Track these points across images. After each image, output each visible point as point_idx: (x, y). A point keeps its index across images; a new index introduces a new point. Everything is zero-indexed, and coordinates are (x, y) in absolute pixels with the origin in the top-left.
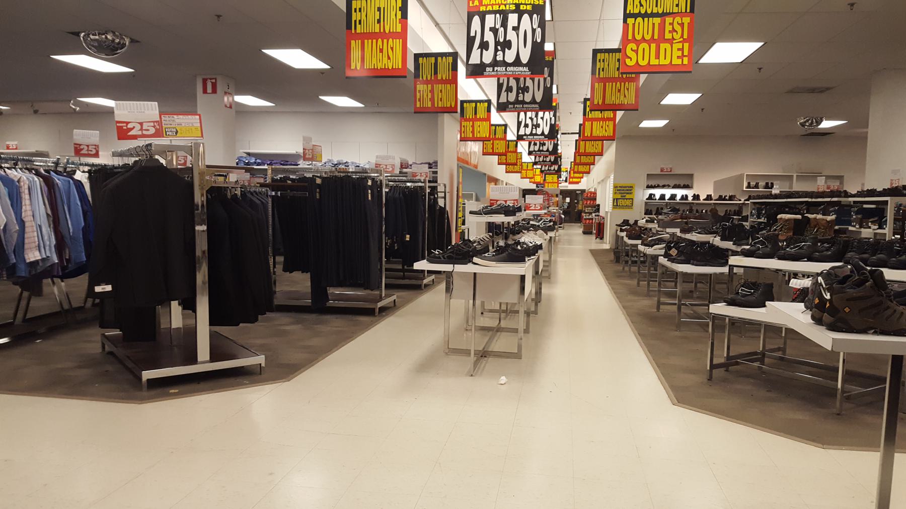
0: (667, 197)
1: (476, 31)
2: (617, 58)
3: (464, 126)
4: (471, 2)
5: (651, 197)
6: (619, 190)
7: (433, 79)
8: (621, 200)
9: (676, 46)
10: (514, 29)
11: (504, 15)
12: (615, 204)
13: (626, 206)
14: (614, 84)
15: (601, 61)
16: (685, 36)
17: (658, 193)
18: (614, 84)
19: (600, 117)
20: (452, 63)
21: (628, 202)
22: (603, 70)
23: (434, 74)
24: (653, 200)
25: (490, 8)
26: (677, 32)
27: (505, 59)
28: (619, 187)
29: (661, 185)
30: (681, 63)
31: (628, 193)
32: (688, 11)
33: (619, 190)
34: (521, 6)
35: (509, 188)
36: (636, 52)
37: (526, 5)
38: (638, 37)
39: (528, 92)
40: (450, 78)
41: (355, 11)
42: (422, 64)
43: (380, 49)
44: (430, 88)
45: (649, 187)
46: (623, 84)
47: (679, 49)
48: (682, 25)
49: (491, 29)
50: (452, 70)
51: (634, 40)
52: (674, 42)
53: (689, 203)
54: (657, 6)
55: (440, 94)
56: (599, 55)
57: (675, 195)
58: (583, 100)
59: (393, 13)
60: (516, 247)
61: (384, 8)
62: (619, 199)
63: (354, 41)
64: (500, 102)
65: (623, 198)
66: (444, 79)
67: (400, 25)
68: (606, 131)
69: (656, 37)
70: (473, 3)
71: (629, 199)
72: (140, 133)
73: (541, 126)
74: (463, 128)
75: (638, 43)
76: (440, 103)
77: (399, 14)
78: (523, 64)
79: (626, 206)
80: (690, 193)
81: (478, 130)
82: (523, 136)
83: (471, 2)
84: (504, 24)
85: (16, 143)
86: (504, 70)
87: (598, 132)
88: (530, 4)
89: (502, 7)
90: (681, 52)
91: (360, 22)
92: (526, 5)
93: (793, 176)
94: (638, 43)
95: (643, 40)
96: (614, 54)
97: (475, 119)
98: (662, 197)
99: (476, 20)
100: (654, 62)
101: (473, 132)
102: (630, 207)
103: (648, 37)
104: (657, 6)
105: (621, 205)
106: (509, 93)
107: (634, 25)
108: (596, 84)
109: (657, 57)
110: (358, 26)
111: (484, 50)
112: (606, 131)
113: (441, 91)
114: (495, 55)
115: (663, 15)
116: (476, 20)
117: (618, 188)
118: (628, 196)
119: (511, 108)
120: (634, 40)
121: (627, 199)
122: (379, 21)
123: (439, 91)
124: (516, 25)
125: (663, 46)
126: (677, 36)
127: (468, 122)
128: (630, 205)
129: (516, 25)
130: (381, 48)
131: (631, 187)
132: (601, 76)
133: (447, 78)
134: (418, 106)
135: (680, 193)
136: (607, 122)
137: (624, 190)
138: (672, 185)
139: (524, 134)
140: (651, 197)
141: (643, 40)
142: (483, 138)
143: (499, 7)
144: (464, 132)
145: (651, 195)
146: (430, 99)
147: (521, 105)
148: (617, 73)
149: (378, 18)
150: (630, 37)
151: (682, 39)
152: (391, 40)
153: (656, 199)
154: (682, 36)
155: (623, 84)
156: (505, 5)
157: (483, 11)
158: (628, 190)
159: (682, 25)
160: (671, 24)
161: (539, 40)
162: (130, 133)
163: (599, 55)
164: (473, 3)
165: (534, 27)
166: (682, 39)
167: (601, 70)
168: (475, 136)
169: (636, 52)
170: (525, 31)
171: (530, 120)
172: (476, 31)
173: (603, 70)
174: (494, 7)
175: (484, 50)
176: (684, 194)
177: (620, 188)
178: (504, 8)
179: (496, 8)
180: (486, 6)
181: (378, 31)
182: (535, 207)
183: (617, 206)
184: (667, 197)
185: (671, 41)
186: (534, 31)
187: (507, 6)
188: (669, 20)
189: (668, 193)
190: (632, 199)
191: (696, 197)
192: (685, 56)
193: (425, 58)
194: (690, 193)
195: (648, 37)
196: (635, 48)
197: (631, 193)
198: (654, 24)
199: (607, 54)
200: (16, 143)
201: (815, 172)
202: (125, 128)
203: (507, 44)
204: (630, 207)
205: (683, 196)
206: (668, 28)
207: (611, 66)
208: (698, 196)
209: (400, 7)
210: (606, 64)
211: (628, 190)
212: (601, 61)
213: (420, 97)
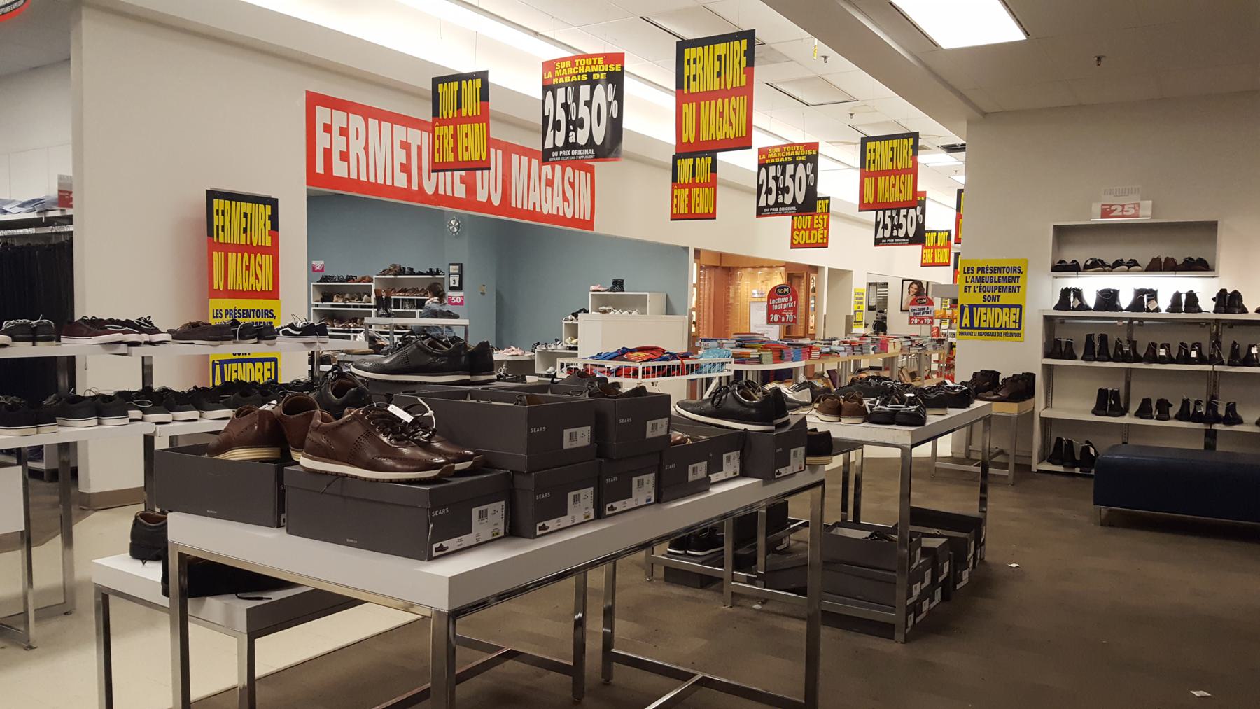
0: (1125, 300)
2: (891, 146)
3: (677, 196)
4: (545, 74)
5: (1067, 298)
6: (979, 279)
8: (984, 310)
9: (820, 232)
11: (784, 165)
12: (966, 321)
13: (1001, 328)
14: (888, 178)
15: (872, 151)
17: (1090, 286)
18: (888, 178)
19: (890, 168)
21: (1007, 318)
22: (874, 162)
23: (692, 177)
24: (1148, 310)
25: (773, 161)
27: (578, 141)
28: (979, 269)
29: (1180, 261)
31: (1005, 289)
33: (979, 279)
36: (799, 235)
38: (800, 227)
39: (788, 193)
41: (218, 214)
43: (246, 266)
44: (687, 192)
45: (1061, 267)
48: (823, 220)
49: (773, 178)
50: (711, 172)
53: (1208, 322)
55: (697, 199)
56: (868, 144)
57: (1153, 294)
58: (860, 141)
59: (262, 223)
61: (251, 214)
62: (978, 306)
64: (760, 205)
65: (991, 303)
66: (702, 182)
68: (901, 192)
69: (809, 227)
71: (1010, 307)
72: (1121, 214)
74: (675, 200)
75: (799, 231)
76: (697, 208)
77: (269, 223)
79: (1001, 328)
80: (1205, 289)
81: (697, 202)
82: (764, 207)
83: (545, 74)
84: (783, 173)
85: (322, 263)
86: (569, 154)
87: (887, 196)
89: (782, 160)
94: (799, 231)
96: (887, 142)
97: (692, 185)
98: (1108, 299)
99: (763, 170)
101: (689, 206)
102: (1014, 330)
103: (805, 227)
105: (983, 325)
108: (866, 180)
112: (901, 192)
113: (699, 195)
114: (777, 198)
117: (975, 275)
118: (1005, 298)
121: (1002, 307)
124: (792, 173)
125: (813, 232)
126: (820, 226)
127: (683, 190)
128: (1013, 325)
129: (792, 173)
131: (1015, 269)
132: (872, 169)
135: (1167, 286)
136: (903, 176)
137: (992, 280)
138: (1145, 261)
139: (765, 205)
140: (1067, 298)
144: (676, 206)
145: (1065, 293)
147: (569, 152)
148: (890, 164)
153: (1157, 310)
154: (823, 226)
155: (898, 177)
158: (1004, 279)
159: (823, 220)
160: (818, 219)
162: (1113, 214)
163: (868, 144)
167: (872, 161)
168: (693, 212)
169: (799, 235)
173: (874, 162)
176: (1184, 290)
177: (980, 274)
178: (576, 80)
179: (777, 160)
180: (771, 159)
181: (244, 243)
182: (1122, 211)
183: (972, 327)
184: (1125, 300)
185: (817, 229)
189: (1126, 286)
190: (1020, 307)
191: (1229, 301)
193: (683, 160)
194: (1205, 289)
195: (805, 227)
197: (1014, 289)
199: (878, 143)
200: (322, 263)
202: (67, 197)
204: (1014, 330)
205: (1177, 296)
206: (816, 222)
207: (884, 157)
208: (1236, 296)
210: (878, 154)
211: (1004, 279)
212: (872, 151)
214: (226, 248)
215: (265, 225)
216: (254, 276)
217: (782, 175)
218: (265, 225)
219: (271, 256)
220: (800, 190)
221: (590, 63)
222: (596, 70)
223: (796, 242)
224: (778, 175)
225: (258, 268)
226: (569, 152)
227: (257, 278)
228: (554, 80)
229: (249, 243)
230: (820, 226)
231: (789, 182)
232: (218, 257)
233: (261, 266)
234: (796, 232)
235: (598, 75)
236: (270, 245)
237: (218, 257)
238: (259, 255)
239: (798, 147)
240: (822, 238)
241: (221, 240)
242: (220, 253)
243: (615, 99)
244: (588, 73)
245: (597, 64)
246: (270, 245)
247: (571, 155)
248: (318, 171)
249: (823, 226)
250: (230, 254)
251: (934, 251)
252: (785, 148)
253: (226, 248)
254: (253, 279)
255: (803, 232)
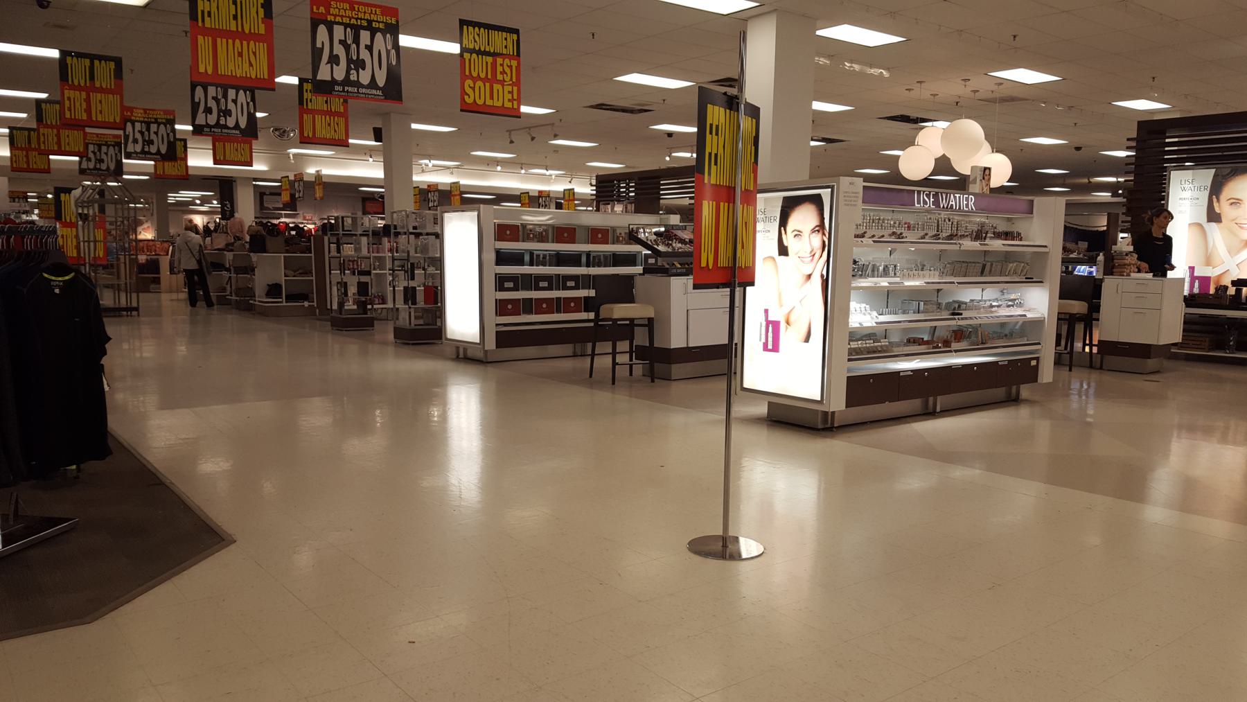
1: (323, 42)
4: (315, 7)
7: (88, 85)
10: (367, 47)
15: (309, 91)
16: (514, 80)
20: (114, 69)
26: (506, 73)
27: (360, 80)
30: (511, 107)
32: (515, 54)
34: (374, 23)
35: (857, 201)
36: (473, 89)
37: (379, 22)
38: (475, 74)
40: (113, 87)
42: (71, 65)
43: (238, 52)
46: (332, 118)
47: (509, 92)
48: (511, 67)
49: (213, 98)
50: (115, 78)
51: (471, 77)
52: (505, 83)
54: (488, 45)
55: (99, 105)
59: (254, 10)
60: (1119, 229)
63: (202, 37)
67: (263, 25)
69: (489, 77)
70: (318, 9)
73: (106, 162)
75: (475, 80)
77: (261, 11)
78: (378, 86)
81: (67, 141)
82: (86, 169)
83: (315, 7)
86: (356, 91)
88: (383, 22)
90: (511, 95)
91: (209, 13)
92: (379, 22)
93: (311, 253)
95: (478, 77)
100: (489, 102)
103: (483, 75)
104: (488, 45)
106: (208, 115)
107: (470, 60)
109: (492, 97)
110: (207, 19)
111: (334, 65)
113: (101, 102)
115: (495, 55)
116: (322, 31)
119: (338, 91)
120: (471, 77)
122: (235, 17)
123: (98, 101)
125: (496, 87)
126: (507, 78)
130: (240, 50)
133: (109, 87)
134: (68, 115)
141: (478, 77)
142: (41, 169)
143: (350, 21)
146: (85, 109)
147: (356, 89)
149: (234, 13)
150: (467, 73)
151: (511, 82)
152: (252, 43)
154: (511, 79)
155: (332, 118)
156: (357, 19)
157: (331, 21)
159: (511, 67)
160: (502, 65)
161: (394, 63)
164: (318, 9)
165: (248, 101)
166: (511, 82)
169: (473, 89)
170: (242, 104)
171: (92, 154)
172: (323, 42)
174: (344, 19)
175: (334, 65)
179: (346, 20)
181: (235, 29)
185: (502, 83)
186: (248, 103)
187: (359, 21)
188: (499, 60)
192: (515, 100)
195: (483, 75)
196: (472, 85)
198: (487, 63)
201: (587, 238)
203: (360, 64)
206: (499, 69)
209: (262, 4)
213: (70, 105)
214: (215, 34)
215: (257, 13)
216: (248, 62)
217: (223, 97)
218: (257, 13)
219: (265, 45)
220: (380, 51)
221: (370, 12)
222: (375, 19)
223: (469, 100)
224: (219, 97)
225: (253, 63)
226: (356, 89)
227: (251, 65)
228: (329, 17)
229: (240, 29)
230: (507, 78)
231: (364, 54)
232: (203, 42)
233: (254, 54)
234: (469, 82)
235: (377, 24)
236: (263, 33)
237: (203, 42)
238: (252, 42)
239: (374, 9)
240: (511, 100)
241: (208, 25)
242: (206, 38)
243: (393, 48)
244: (367, 20)
245: (376, 13)
246: (263, 33)
247: (222, 132)
248: (540, 283)
249: (511, 79)
250: (219, 40)
251: (88, 96)
252: (356, 7)
253: (215, 34)
254: (246, 65)
255: (479, 84)
